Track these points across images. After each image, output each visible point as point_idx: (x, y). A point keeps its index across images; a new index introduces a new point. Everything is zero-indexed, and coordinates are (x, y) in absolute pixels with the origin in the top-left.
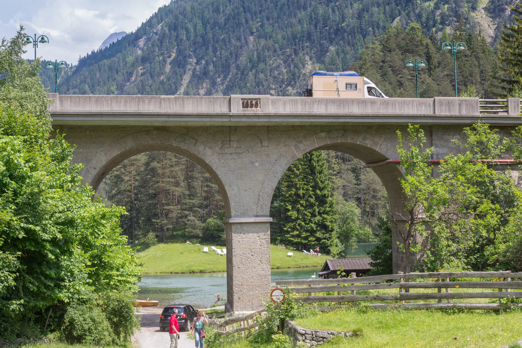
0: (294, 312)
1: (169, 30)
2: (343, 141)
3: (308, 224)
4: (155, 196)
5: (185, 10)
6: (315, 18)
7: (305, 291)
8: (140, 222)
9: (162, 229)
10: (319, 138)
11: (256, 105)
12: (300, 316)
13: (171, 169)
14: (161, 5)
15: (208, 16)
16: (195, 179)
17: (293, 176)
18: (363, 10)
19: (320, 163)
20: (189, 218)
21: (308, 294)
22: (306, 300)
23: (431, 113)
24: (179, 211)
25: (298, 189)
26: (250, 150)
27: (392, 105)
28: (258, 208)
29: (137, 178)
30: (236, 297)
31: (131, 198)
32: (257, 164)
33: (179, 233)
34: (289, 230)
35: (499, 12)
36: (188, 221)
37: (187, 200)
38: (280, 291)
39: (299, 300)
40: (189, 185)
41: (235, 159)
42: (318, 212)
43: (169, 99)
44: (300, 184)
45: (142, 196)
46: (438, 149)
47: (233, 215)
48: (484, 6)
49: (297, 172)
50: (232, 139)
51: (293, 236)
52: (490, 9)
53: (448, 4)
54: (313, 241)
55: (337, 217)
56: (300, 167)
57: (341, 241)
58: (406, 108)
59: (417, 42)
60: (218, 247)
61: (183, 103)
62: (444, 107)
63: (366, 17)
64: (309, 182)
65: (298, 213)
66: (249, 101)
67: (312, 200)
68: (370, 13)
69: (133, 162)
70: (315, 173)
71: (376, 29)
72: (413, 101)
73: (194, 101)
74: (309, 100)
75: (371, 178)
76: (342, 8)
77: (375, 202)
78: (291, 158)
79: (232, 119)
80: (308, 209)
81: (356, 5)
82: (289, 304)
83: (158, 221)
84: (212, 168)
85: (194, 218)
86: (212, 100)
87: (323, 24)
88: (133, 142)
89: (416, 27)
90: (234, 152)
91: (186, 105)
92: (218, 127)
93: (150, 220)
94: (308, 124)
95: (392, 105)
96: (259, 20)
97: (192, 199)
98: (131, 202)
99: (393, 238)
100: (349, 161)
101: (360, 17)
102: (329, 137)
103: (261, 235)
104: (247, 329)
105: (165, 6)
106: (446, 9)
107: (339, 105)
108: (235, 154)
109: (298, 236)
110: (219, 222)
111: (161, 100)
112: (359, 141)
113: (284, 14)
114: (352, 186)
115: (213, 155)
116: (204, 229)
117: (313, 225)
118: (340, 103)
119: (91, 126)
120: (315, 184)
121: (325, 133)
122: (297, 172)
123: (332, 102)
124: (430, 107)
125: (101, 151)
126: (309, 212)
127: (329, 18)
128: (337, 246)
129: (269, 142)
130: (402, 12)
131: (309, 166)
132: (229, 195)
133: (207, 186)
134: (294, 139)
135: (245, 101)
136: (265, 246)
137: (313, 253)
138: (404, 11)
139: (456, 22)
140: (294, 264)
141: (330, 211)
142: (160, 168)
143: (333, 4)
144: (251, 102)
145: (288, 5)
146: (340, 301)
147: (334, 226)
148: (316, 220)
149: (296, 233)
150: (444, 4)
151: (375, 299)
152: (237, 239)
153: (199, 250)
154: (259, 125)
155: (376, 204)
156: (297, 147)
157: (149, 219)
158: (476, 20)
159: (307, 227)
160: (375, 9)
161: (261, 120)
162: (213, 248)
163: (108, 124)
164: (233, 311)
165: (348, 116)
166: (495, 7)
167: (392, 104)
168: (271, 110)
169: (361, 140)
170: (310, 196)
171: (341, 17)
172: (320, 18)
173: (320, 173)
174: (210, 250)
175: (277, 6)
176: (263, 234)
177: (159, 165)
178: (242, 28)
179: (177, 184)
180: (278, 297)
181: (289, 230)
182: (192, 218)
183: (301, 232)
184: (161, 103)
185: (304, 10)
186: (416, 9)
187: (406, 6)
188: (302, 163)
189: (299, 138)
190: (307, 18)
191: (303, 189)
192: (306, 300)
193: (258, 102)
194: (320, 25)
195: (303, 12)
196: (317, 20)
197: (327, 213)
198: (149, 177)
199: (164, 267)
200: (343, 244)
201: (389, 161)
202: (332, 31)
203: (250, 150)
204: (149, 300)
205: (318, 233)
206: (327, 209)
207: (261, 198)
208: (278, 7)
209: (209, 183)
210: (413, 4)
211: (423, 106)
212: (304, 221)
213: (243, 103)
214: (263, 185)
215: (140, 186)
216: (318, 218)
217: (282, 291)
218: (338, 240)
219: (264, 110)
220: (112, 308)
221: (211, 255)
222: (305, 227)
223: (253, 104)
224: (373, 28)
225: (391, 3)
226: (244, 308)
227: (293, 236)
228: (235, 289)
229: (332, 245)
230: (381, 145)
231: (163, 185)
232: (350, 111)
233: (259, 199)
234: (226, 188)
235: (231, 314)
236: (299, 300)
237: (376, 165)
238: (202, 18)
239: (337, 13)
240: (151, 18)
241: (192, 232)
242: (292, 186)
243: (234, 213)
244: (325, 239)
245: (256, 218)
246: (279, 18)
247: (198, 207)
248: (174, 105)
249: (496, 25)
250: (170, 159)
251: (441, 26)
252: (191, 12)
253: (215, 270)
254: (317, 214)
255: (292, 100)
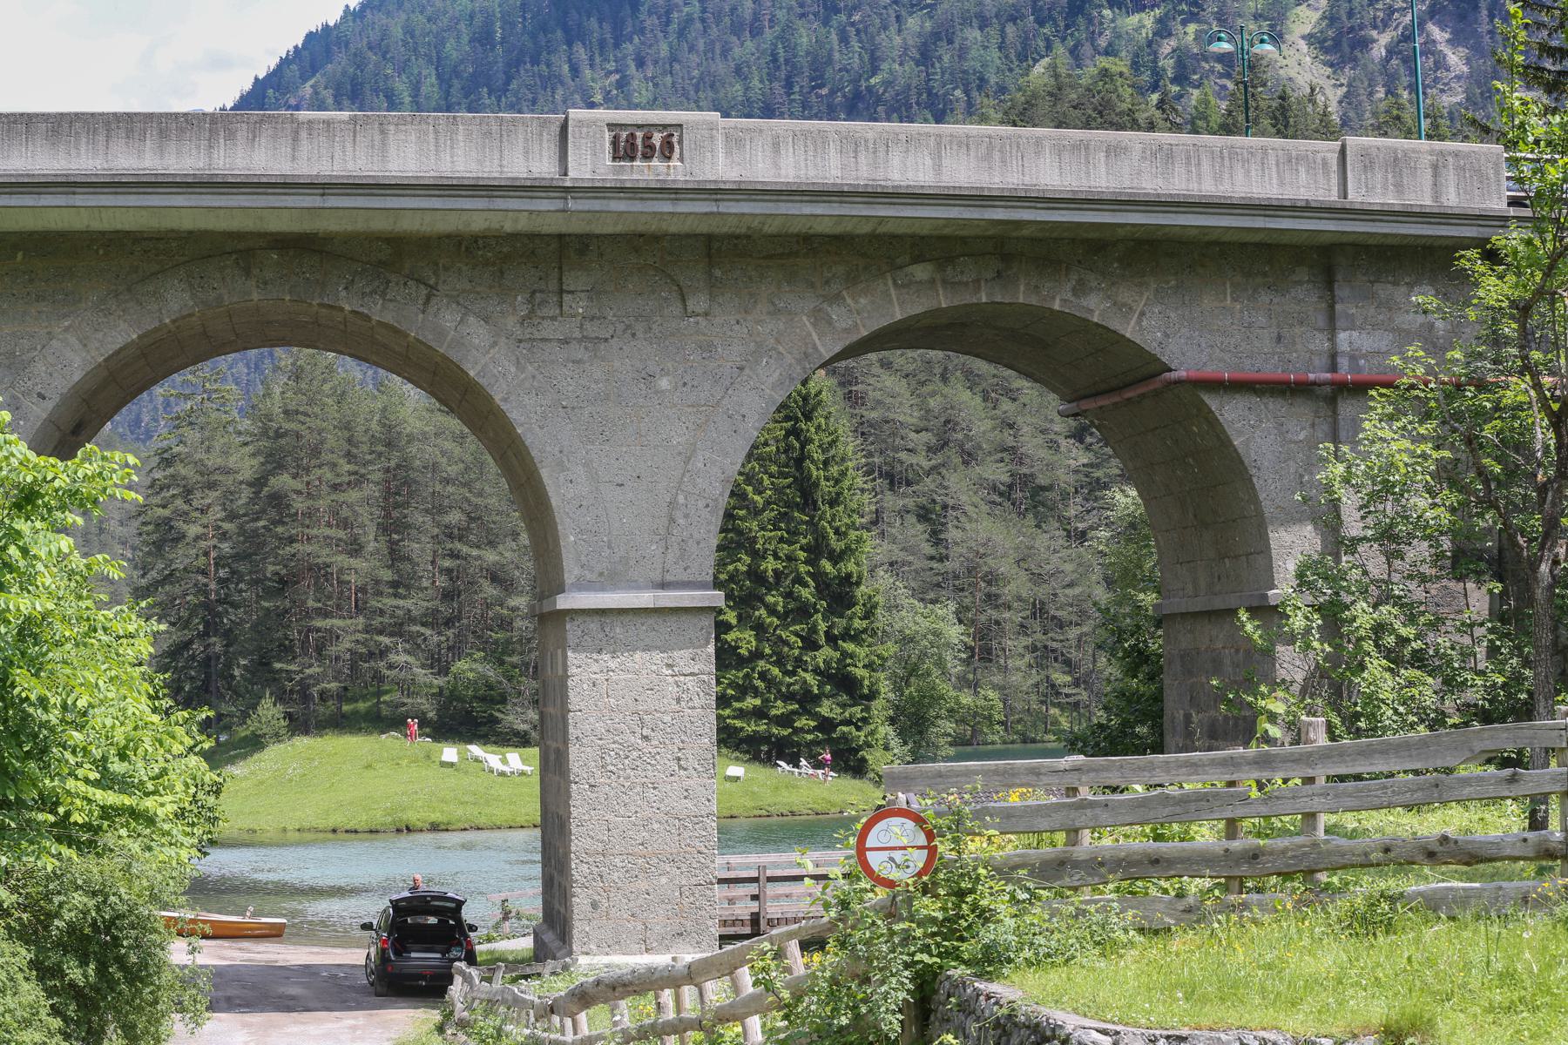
0: (1004, 929)
1: (335, 97)
2: (998, 299)
3: (793, 673)
4: (284, 584)
5: (385, 34)
6: (787, 61)
7: (1043, 824)
8: (237, 672)
9: (305, 697)
10: (903, 286)
11: (667, 150)
12: (1027, 953)
13: (334, 497)
14: (314, 25)
15: (455, 54)
16: (414, 532)
17: (742, 513)
18: (936, 36)
19: (834, 470)
20: (393, 658)
21: (1061, 837)
22: (1054, 870)
23: (1332, 196)
24: (360, 637)
25: (757, 556)
26: (639, 328)
27: (1188, 163)
28: (670, 556)
29: (226, 526)
30: (580, 902)
31: (206, 593)
32: (664, 383)
33: (362, 706)
34: (730, 692)
35: (1353, 48)
36: (391, 667)
37: (386, 601)
38: (910, 824)
39: (1015, 868)
40: (392, 552)
41: (579, 362)
42: (826, 633)
43: (328, 123)
44: (764, 538)
45: (242, 586)
46: (1355, 334)
47: (569, 578)
48: (1307, 29)
49: (757, 498)
50: (570, 282)
51: (741, 714)
52: (1325, 40)
53: (1198, 22)
54: (809, 732)
55: (890, 649)
56: (766, 482)
57: (903, 734)
58: (1240, 176)
59: (1121, 114)
60: (490, 748)
61: (384, 143)
62: (1379, 176)
63: (946, 58)
64: (794, 533)
65: (759, 639)
66: (639, 134)
67: (806, 593)
68: (957, 45)
69: (216, 477)
70: (815, 502)
71: (975, 94)
72: (1264, 149)
73: (426, 133)
74: (870, 135)
75: (983, 536)
76: (871, 29)
77: (994, 614)
78: (799, 361)
79: (571, 204)
80: (794, 622)
81: (912, 23)
82: (961, 894)
83: (293, 667)
84: (489, 399)
85: (410, 659)
86: (495, 128)
87: (812, 80)
88: (187, 296)
89: (1114, 69)
90: (577, 334)
91: (392, 151)
92: (515, 236)
93: (268, 664)
94: (866, 229)
95: (1188, 163)
96: (611, 66)
97: (404, 597)
98: (207, 606)
99: (1167, 679)
100: (909, 484)
101: (925, 57)
102: (944, 282)
103: (682, 657)
104: (698, 1025)
105: (326, 27)
106: (1191, 37)
107: (988, 157)
108: (580, 341)
109: (759, 714)
110: (491, 672)
111: (297, 127)
112: (1060, 299)
113: (691, 49)
114: (918, 564)
115: (495, 344)
116: (441, 693)
117: (809, 677)
118: (991, 147)
119: (32, 233)
120: (816, 540)
121: (929, 267)
122: (757, 498)
123: (960, 144)
124: (1326, 172)
125: (66, 330)
126: (796, 634)
127: (830, 61)
128: (887, 748)
129: (712, 298)
130: (1057, 44)
131: (796, 479)
132: (554, 502)
133: (454, 555)
134: (812, 285)
135: (624, 135)
136: (697, 703)
137: (811, 771)
138: (1063, 39)
139: (1221, 76)
140: (750, 804)
141: (865, 631)
142: (299, 493)
143: (844, 18)
144: (648, 137)
145: (703, 20)
146: (1240, 872)
147: (878, 680)
148: (820, 661)
149: (751, 702)
150: (1184, 23)
151: (1431, 855)
152: (585, 677)
153: (428, 757)
154: (673, 229)
155: (997, 623)
156: (819, 317)
157: (263, 664)
158: (1281, 72)
159: (789, 685)
160: (973, 34)
161: (684, 207)
162: (475, 750)
163: (96, 225)
164: (570, 953)
165: (1019, 199)
166: (1340, 34)
167: (1188, 158)
168: (720, 167)
169: (1069, 296)
170: (799, 580)
171: (866, 58)
172: (803, 61)
173: (833, 503)
174: (463, 759)
175: (668, 22)
176: (686, 653)
177: (298, 485)
178: (560, 92)
179: (355, 548)
180: (898, 855)
181: (730, 692)
182: (403, 658)
183: (767, 700)
184: (296, 139)
185: (753, 36)
186: (1101, 34)
187: (1067, 27)
188: (774, 469)
189: (827, 282)
190: (762, 61)
191: (776, 557)
192: (1054, 870)
193: (675, 140)
194: (802, 82)
195: (748, 43)
196: (794, 66)
197: (856, 638)
198: (262, 523)
199: (312, 810)
200: (905, 743)
201: (1173, 375)
202: (839, 99)
203: (639, 328)
204: (254, 915)
205: (826, 703)
206: (858, 624)
207: (678, 515)
208: (674, 27)
209: (458, 545)
210: (1090, 21)
211: (1302, 170)
212: (780, 663)
213: (615, 142)
214: (687, 462)
215: (237, 557)
216: (825, 654)
217: (918, 820)
218: (890, 730)
219: (696, 171)
220: (70, 924)
221: (466, 773)
222: (781, 683)
223: (652, 147)
224: (967, 92)
225: (1022, 17)
226: (615, 944)
227: (741, 714)
228: (579, 870)
229: (870, 746)
230: (1142, 314)
231: (309, 549)
232: (1027, 180)
233: (672, 520)
234: (544, 473)
235: (565, 968)
236: (1015, 868)
237: (1117, 399)
238: (439, 64)
239: (856, 45)
240: (284, 63)
241: (404, 704)
242: (740, 546)
243: (576, 571)
244: (848, 722)
245: (661, 593)
246: (674, 59)
247: (423, 625)
248: (349, 146)
249: (1345, 89)
250: (334, 465)
251: (1175, 89)
252: (405, 44)
253: (482, 821)
254: (822, 640)
255: (806, 134)
